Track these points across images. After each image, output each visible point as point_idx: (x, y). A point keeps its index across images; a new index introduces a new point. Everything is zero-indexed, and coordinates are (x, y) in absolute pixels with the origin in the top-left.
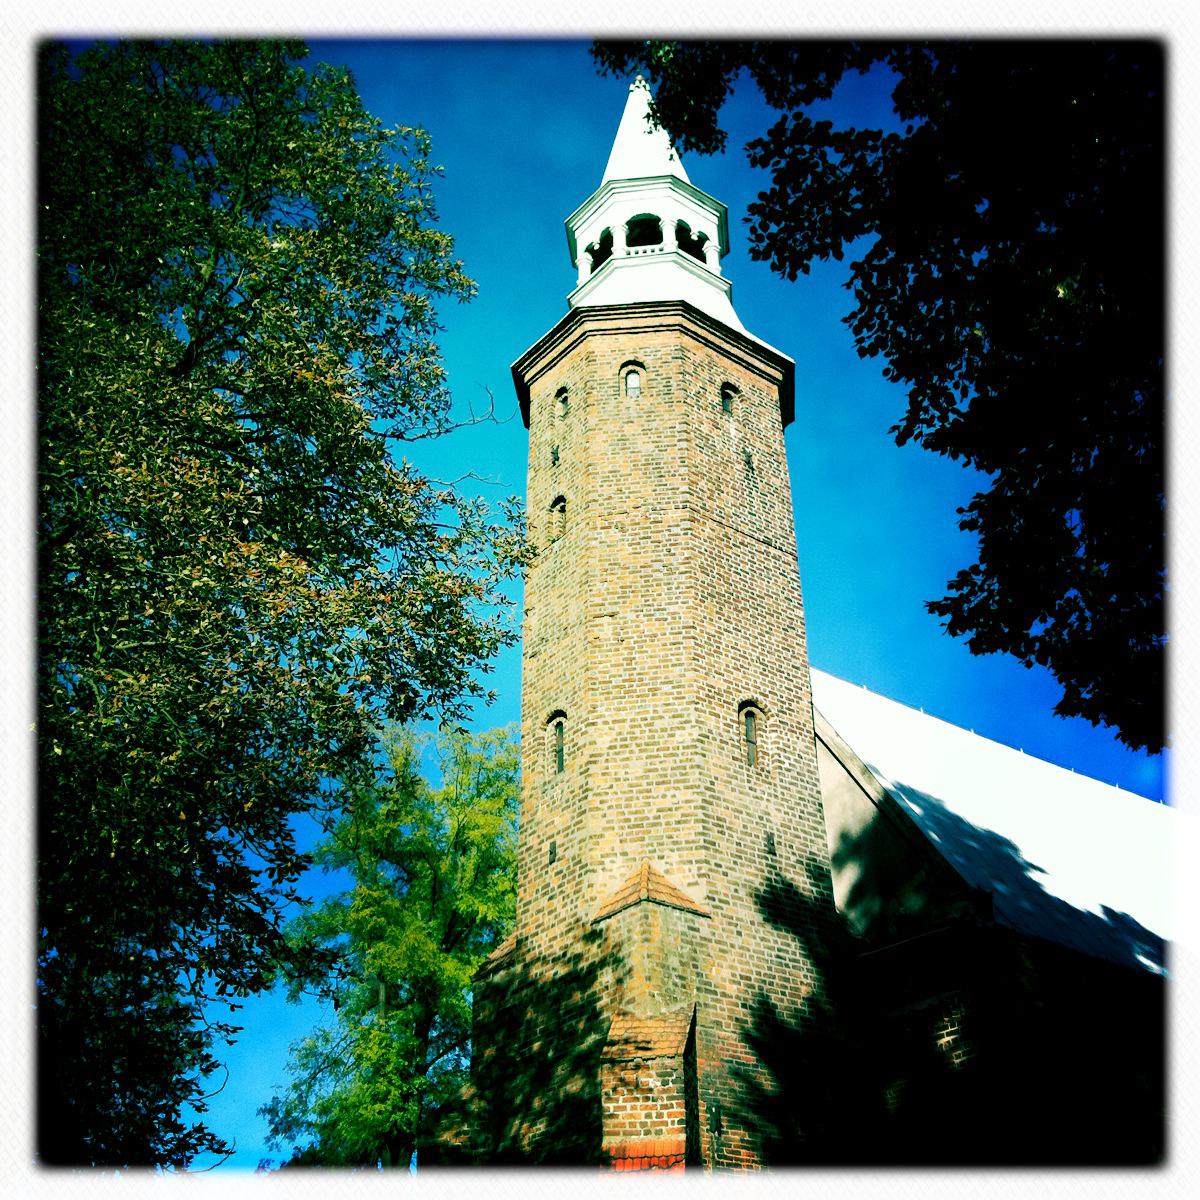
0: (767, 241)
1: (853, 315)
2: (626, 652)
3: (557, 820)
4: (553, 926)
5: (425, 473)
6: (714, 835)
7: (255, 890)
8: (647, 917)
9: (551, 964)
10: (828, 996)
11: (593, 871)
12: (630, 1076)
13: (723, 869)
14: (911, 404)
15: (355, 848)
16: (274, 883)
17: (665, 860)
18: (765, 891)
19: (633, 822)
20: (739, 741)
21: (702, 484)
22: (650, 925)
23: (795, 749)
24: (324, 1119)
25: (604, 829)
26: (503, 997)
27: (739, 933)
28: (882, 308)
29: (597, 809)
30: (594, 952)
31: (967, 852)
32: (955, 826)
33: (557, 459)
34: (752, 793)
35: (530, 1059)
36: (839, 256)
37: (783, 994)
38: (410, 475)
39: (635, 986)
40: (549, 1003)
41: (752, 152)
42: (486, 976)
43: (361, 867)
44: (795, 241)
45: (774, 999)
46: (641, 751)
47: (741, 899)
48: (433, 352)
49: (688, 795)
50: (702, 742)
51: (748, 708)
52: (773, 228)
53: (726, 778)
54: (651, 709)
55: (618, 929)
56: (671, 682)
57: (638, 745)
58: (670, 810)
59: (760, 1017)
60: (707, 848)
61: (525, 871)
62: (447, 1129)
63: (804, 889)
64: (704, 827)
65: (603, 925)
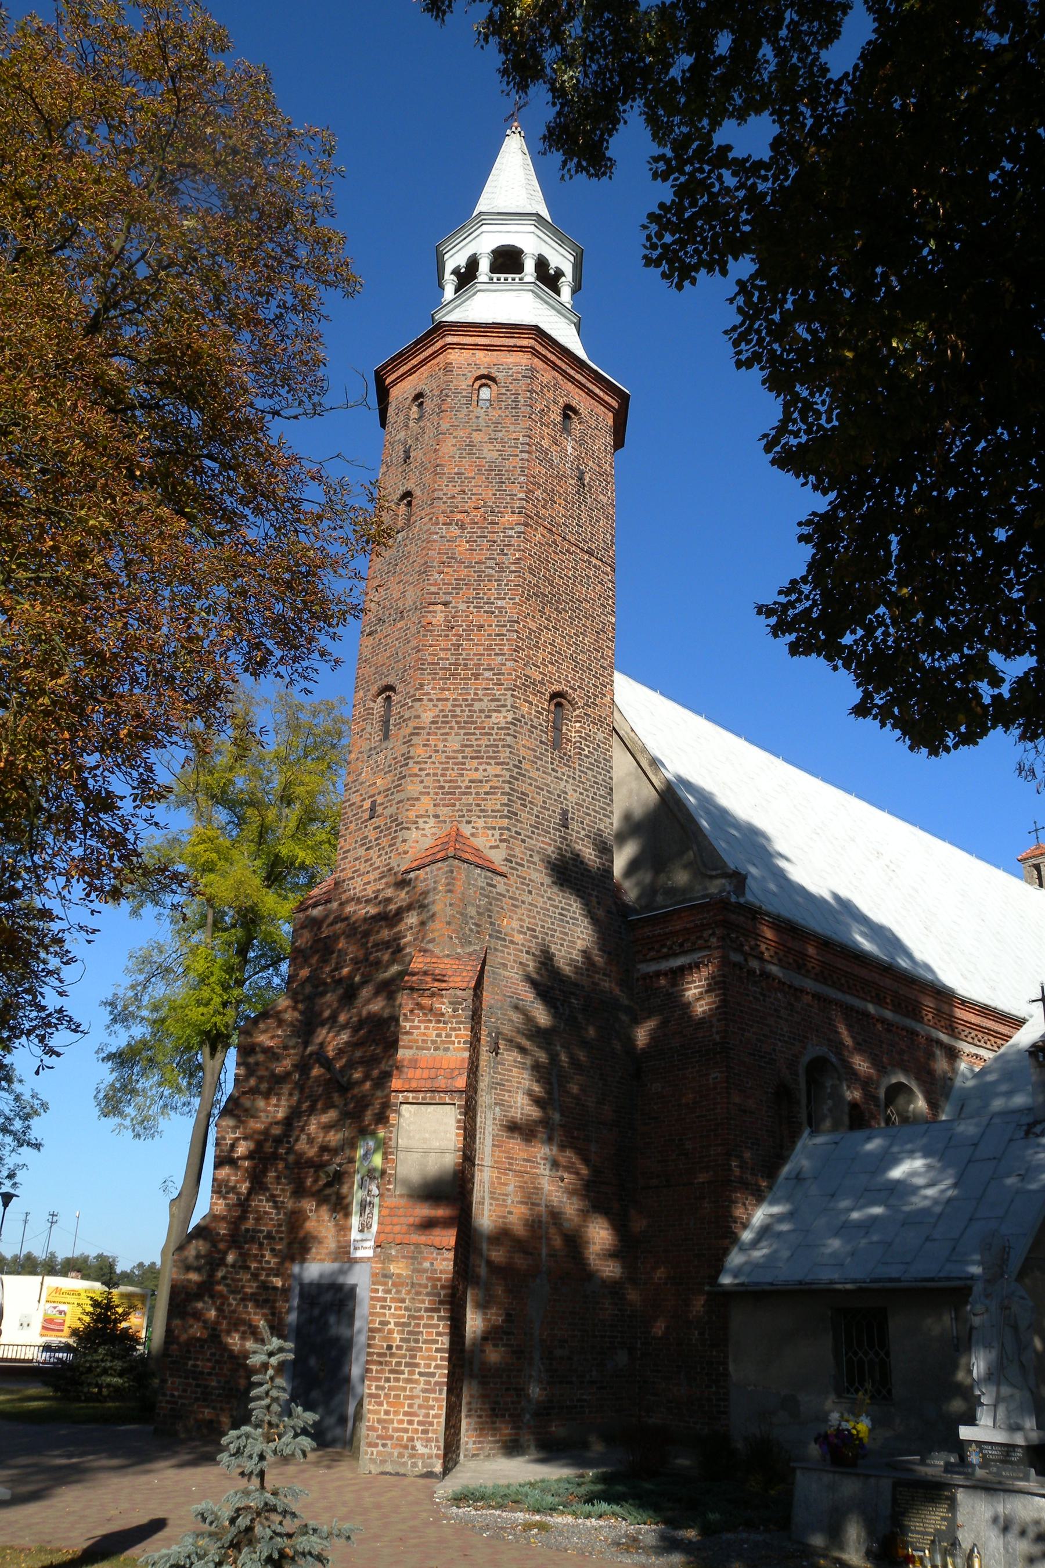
0: (659, 250)
1: (734, 329)
2: (454, 638)
3: (379, 782)
4: (368, 872)
5: (298, 450)
6: (517, 806)
7: (120, 813)
8: (452, 872)
9: (363, 905)
10: (600, 950)
11: (408, 829)
12: (426, 1002)
13: (522, 837)
14: (784, 412)
15: (194, 792)
16: (135, 808)
17: (473, 824)
18: (556, 859)
19: (446, 790)
20: (547, 727)
21: (538, 493)
22: (454, 879)
23: (595, 739)
24: (155, 1015)
25: (421, 793)
26: (320, 928)
27: (530, 892)
28: (761, 325)
29: (416, 775)
30: (402, 897)
31: (730, 839)
32: (722, 816)
33: (409, 458)
34: (554, 774)
35: (339, 981)
36: (724, 272)
37: (562, 945)
38: (284, 450)
39: (438, 928)
40: (359, 936)
41: (654, 166)
42: (307, 909)
43: (198, 809)
44: (686, 253)
45: (553, 949)
46: (460, 728)
47: (534, 863)
48: (316, 339)
49: (498, 770)
50: (515, 725)
51: (558, 698)
52: (668, 238)
53: (532, 758)
54: (472, 692)
55: (425, 880)
56: (493, 669)
57: (457, 722)
58: (481, 781)
59: (540, 963)
60: (510, 818)
61: (346, 824)
62: (265, 1031)
63: (589, 859)
64: (509, 800)
65: (412, 875)
